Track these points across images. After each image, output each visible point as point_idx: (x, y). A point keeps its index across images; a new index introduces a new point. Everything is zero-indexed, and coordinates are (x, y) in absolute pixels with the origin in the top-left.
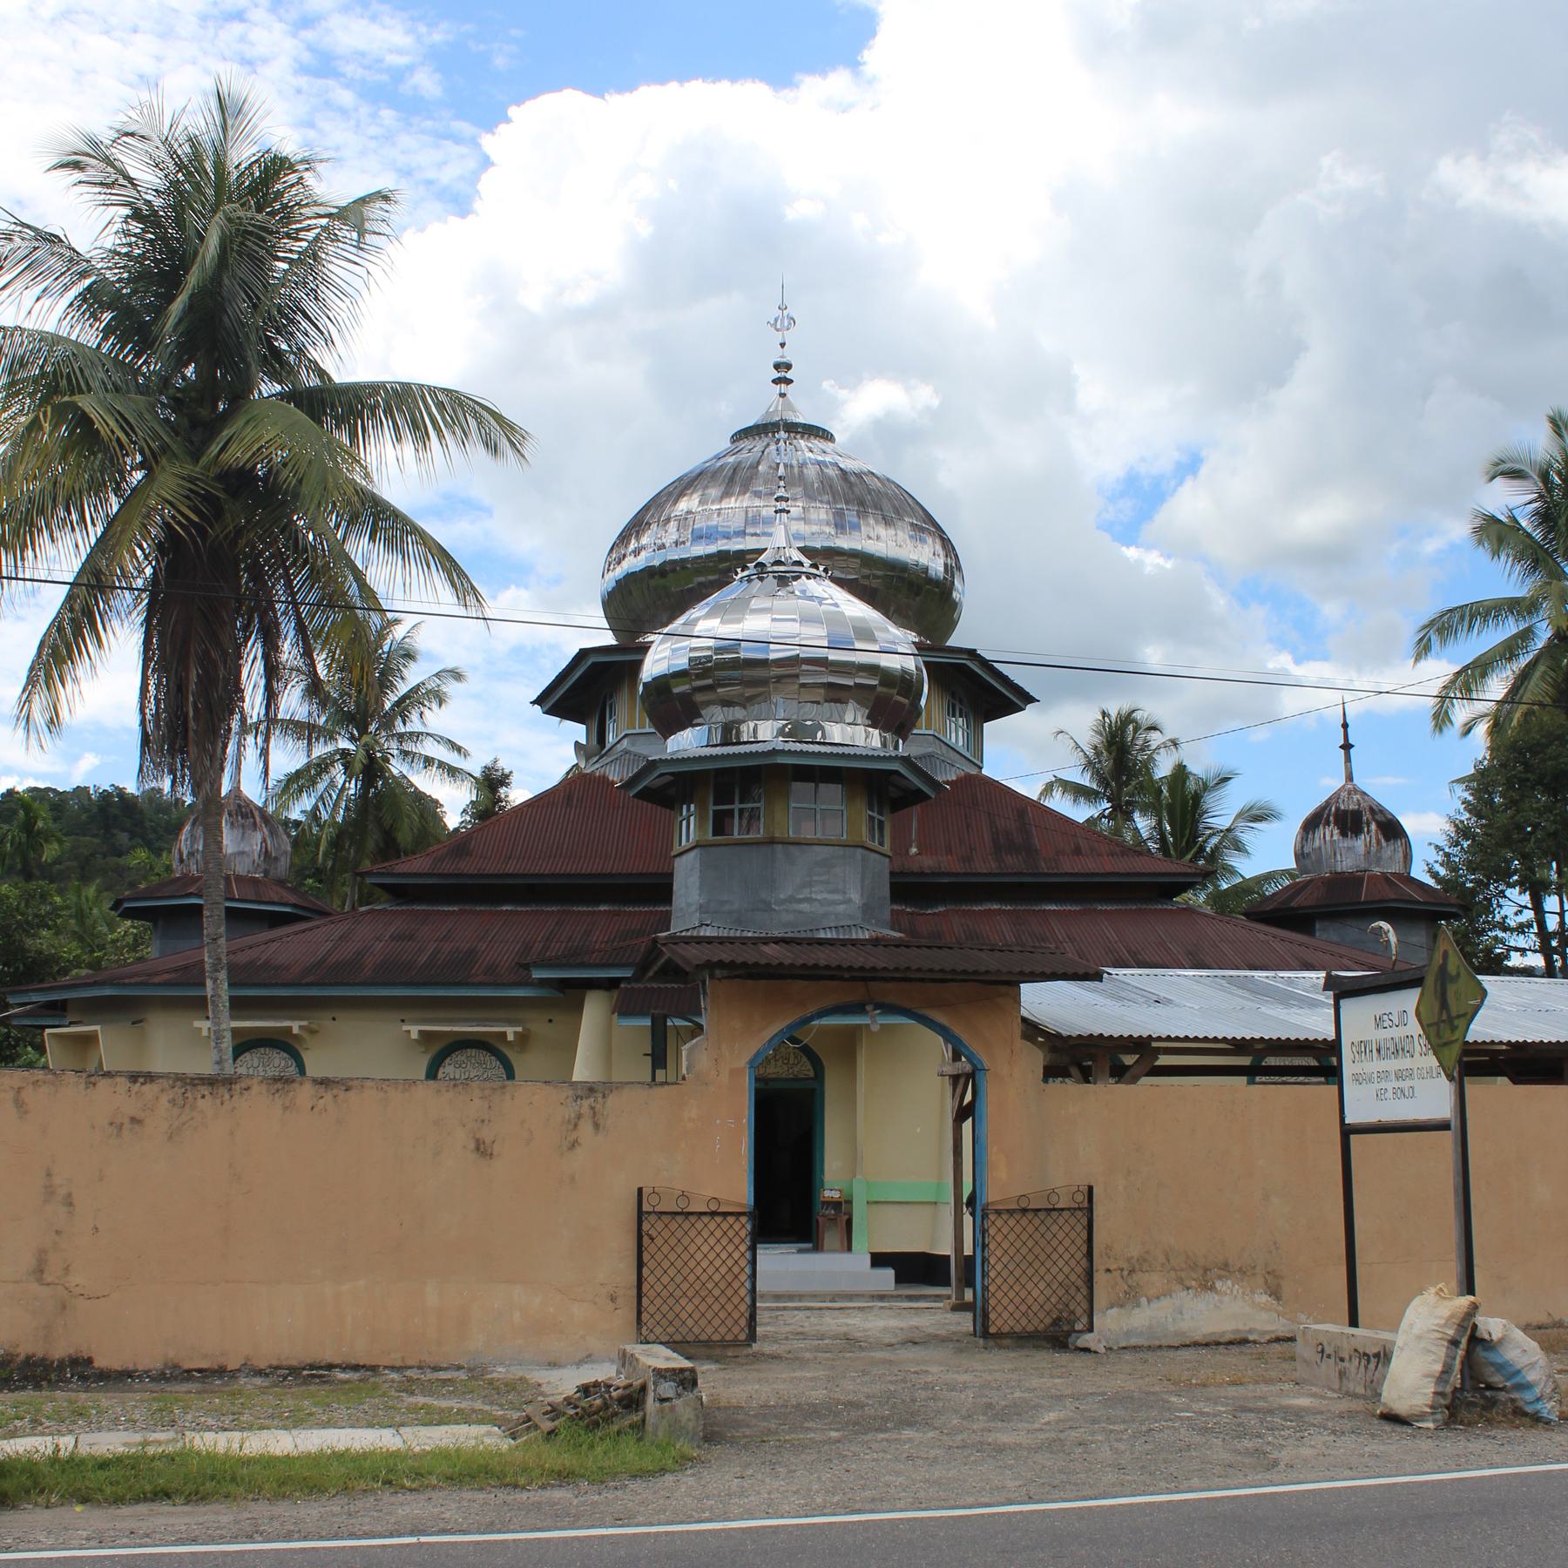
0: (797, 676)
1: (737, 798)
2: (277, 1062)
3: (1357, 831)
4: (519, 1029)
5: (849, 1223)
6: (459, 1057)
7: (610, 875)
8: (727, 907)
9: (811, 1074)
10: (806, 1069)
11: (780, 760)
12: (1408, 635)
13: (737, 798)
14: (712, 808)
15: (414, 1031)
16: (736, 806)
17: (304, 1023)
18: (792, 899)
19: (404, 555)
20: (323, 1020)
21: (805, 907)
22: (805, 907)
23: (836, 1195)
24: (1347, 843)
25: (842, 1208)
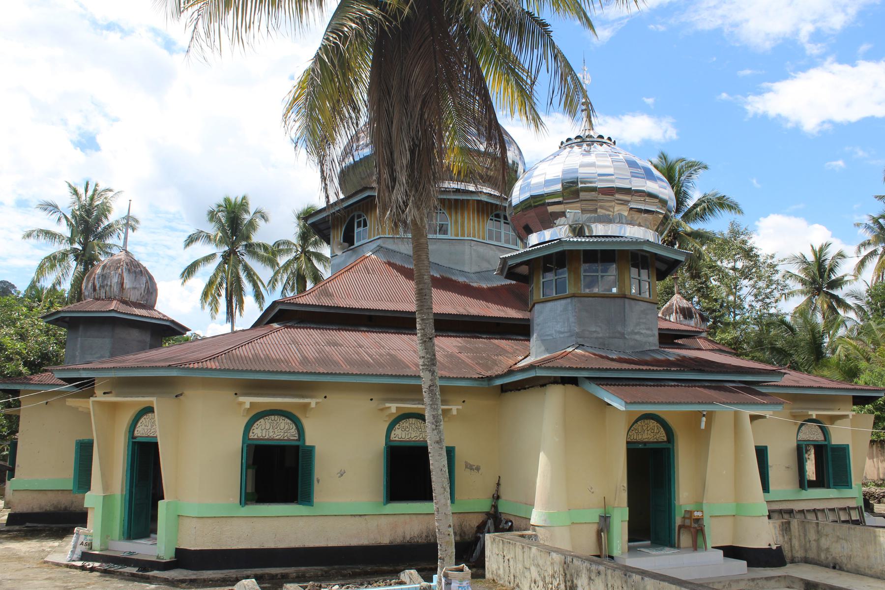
0: (629, 202)
2: (282, 426)
3: (691, 317)
6: (404, 424)
8: (595, 335)
11: (646, 248)
12: (183, 245)
18: (633, 333)
19: (769, 90)
21: (637, 337)
22: (637, 337)
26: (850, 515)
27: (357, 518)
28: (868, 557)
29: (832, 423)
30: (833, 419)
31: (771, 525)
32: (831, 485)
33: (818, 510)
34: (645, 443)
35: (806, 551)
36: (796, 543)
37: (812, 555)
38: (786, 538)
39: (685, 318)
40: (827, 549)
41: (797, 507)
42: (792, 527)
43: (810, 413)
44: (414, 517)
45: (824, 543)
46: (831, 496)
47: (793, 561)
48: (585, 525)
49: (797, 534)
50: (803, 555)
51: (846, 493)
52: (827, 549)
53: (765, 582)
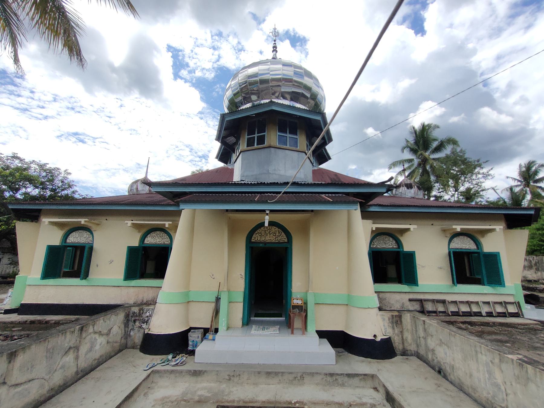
1: (256, 132)
4: (171, 223)
5: (306, 316)
6: (153, 234)
7: (279, 243)
9: (286, 240)
10: (283, 238)
13: (256, 132)
14: (247, 137)
15: (130, 223)
16: (256, 135)
17: (87, 220)
20: (102, 219)
23: (299, 302)
24: (409, 190)
25: (303, 309)
26: (506, 308)
27: (116, 288)
28: (471, 376)
29: (483, 236)
30: (484, 232)
31: (379, 318)
32: (486, 283)
33: (472, 302)
34: (265, 243)
35: (418, 346)
36: (408, 336)
37: (422, 352)
38: (397, 331)
39: (408, 188)
40: (433, 350)
41: (449, 298)
42: (403, 320)
43: (454, 227)
44: (150, 288)
45: (432, 343)
46: (485, 292)
47: (404, 353)
48: (204, 304)
49: (409, 327)
50: (416, 349)
51: (500, 290)
52: (433, 350)
53: (346, 379)
